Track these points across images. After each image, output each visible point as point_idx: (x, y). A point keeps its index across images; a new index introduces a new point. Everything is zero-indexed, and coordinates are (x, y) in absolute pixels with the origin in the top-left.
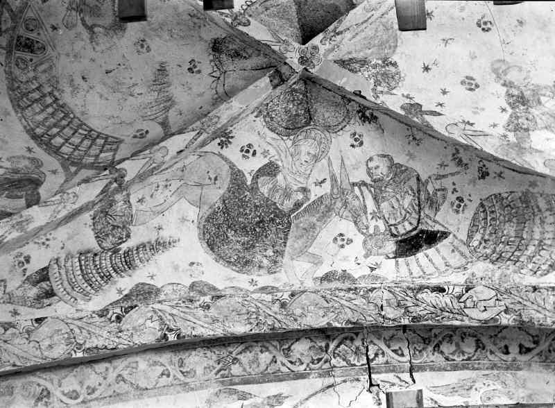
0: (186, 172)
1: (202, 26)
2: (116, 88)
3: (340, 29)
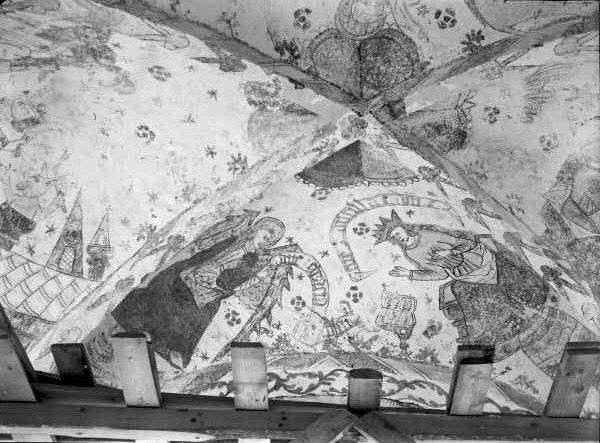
3: (315, 154)
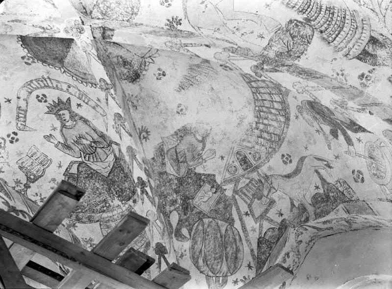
0: (218, 27)
1: (134, 96)
2: (218, 100)
